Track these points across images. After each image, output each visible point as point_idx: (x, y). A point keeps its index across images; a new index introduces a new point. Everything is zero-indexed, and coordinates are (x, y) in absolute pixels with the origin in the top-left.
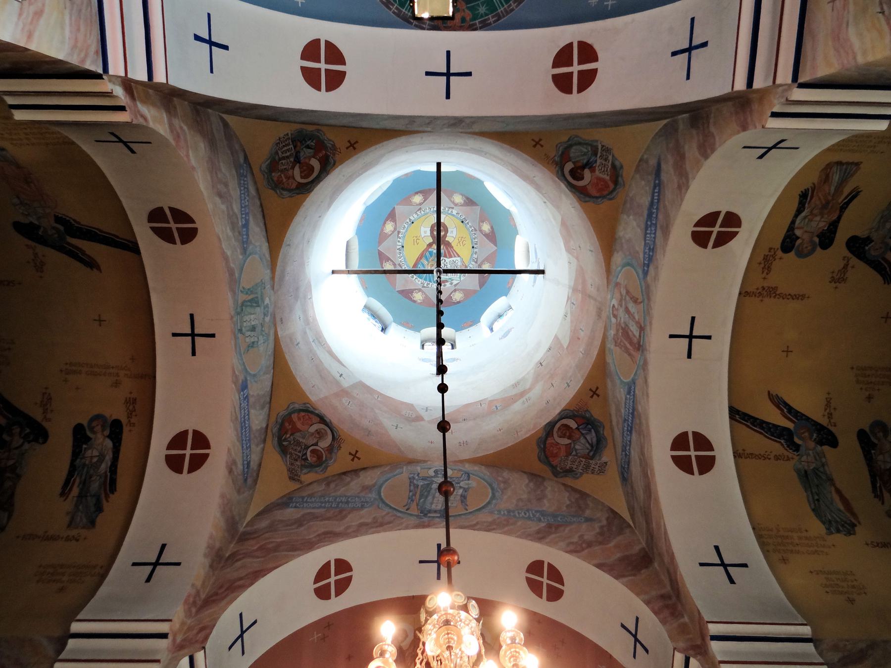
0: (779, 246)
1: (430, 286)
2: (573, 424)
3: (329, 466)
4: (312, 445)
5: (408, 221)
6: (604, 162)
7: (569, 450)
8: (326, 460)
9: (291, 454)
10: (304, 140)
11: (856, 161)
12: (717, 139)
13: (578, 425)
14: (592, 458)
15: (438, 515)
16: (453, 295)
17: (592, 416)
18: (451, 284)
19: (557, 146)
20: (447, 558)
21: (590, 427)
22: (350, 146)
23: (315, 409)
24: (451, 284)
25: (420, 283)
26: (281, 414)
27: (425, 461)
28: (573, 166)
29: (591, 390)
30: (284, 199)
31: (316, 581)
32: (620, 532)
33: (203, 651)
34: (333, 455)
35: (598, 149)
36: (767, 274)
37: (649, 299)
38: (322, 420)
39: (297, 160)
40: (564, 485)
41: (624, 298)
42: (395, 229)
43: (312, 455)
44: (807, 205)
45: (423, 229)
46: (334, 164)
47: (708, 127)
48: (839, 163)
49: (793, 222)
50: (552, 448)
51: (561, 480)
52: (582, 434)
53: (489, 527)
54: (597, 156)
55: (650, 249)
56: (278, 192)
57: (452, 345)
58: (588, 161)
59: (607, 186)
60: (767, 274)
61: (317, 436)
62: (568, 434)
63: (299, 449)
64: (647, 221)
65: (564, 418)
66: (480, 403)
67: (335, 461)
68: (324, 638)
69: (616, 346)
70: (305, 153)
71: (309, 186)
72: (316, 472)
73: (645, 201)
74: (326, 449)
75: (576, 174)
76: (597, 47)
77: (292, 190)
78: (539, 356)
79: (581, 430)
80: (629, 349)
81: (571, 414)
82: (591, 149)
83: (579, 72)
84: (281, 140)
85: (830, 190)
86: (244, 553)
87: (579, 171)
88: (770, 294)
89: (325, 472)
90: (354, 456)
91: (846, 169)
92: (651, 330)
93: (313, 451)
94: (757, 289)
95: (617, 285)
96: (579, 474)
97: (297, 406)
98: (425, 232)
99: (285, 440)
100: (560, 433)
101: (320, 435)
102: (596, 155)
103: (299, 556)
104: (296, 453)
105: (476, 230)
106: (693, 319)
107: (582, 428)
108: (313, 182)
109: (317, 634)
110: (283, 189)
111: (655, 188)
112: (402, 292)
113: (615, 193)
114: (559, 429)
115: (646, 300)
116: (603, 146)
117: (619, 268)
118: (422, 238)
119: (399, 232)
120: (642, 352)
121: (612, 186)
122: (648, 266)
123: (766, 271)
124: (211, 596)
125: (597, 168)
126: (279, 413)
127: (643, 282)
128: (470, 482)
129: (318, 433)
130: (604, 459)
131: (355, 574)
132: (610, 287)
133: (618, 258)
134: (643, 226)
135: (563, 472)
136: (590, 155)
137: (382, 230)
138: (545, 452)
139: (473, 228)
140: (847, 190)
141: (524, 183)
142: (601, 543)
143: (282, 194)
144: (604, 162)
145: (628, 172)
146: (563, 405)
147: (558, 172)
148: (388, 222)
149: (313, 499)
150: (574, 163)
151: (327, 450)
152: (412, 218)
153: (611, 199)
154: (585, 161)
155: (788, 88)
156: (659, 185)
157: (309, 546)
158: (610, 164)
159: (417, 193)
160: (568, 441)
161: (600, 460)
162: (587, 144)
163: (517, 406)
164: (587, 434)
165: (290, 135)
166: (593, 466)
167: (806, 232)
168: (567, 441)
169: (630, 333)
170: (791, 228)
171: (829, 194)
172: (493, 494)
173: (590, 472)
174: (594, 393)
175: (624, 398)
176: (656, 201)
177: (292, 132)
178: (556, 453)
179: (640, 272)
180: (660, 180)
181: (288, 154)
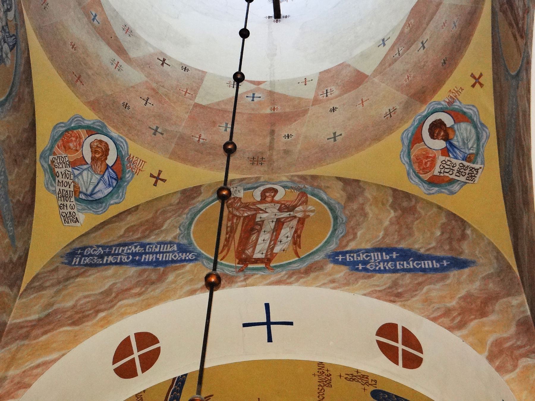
0: (379, 388)
2: (111, 160)
6: (456, 169)
13: (112, 166)
14: (78, 200)
19: (473, 106)
20: (5, 211)
21: (114, 184)
28: (448, 126)
29: (160, 172)
32: (11, 286)
35: (474, 163)
36: (346, 378)
37: (308, 271)
47: (526, 355)
50: (74, 139)
54: (463, 160)
55: (365, 263)
58: (456, 147)
59: (426, 170)
60: (346, 378)
62: (97, 156)
65: (115, 144)
79: (107, 173)
80: (234, 237)
82: (472, 154)
87: (442, 134)
88: (323, 381)
94: (328, 371)
96: (54, 189)
100: (96, 144)
102: (465, 159)
106: (291, 324)
111: (439, 259)
113: (417, 180)
114: (101, 141)
117: (325, 197)
120: (241, 270)
121: (427, 177)
122: (344, 263)
123: (349, 378)
135: (49, 165)
144: (456, 169)
153: (408, 174)
154: (455, 143)
156: (443, 269)
158: (453, 177)
160: (88, 159)
161: (79, 210)
162: (478, 149)
164: (105, 183)
166: (68, 203)
168: (88, 157)
169: (254, 237)
173: (60, 203)
174: (158, 178)
175: (169, 238)
178: (70, 148)
179: (332, 247)
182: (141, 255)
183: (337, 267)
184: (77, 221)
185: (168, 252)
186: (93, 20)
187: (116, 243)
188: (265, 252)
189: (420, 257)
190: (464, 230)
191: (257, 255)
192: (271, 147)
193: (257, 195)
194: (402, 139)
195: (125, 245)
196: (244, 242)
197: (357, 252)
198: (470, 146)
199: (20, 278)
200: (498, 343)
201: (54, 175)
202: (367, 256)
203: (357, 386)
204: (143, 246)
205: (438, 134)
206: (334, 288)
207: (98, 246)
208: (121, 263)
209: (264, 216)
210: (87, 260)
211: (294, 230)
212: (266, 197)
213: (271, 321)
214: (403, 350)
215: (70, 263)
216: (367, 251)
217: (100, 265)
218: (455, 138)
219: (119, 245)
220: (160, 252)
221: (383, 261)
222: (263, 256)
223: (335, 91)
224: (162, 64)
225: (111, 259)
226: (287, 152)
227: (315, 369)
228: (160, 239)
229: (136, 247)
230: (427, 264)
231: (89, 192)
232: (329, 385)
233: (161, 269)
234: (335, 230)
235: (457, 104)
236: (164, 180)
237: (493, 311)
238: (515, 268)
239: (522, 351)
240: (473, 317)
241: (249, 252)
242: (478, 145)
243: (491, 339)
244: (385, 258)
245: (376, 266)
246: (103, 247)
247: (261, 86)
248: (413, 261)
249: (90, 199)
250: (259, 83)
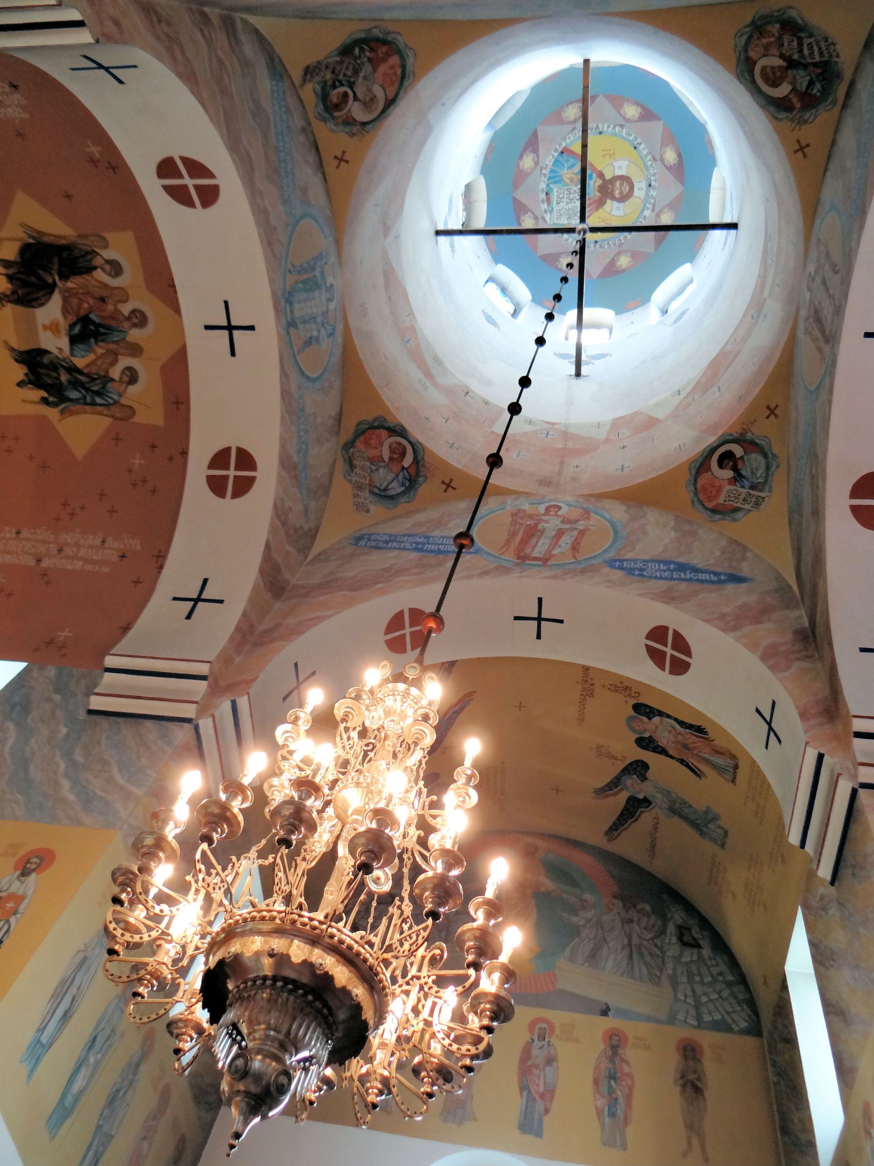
1: (543, 178)
2: (408, 461)
3: (326, 125)
4: (355, 94)
5: (639, 140)
7: (376, 461)
8: (333, 118)
9: (342, 62)
10: (824, 79)
11: (736, 780)
12: (785, 674)
14: (372, 493)
15: (289, 319)
16: (530, 216)
17: (420, 485)
18: (546, 211)
22: (804, 147)
23: (406, 91)
24: (546, 211)
25: (547, 162)
26: (399, 37)
27: (340, 263)
29: (451, 480)
30: (733, 37)
31: (185, 160)
32: (299, 551)
33: (92, 41)
34: (341, 127)
36: (609, 689)
37: (583, 571)
38: (390, 103)
39: (792, 64)
40: (335, 461)
41: (574, 526)
42: (628, 120)
43: (341, 95)
44: (688, 731)
45: (624, 164)
46: (776, 118)
47: (798, 659)
48: (736, 767)
49: (669, 716)
51: (339, 456)
52: (397, 475)
53: (286, 394)
55: (641, 570)
56: (748, 29)
57: (515, 311)
60: (609, 689)
61: (368, 99)
63: (349, 73)
64: (674, 563)
66: (411, 313)
67: (333, 131)
68: (93, 161)
69: (513, 515)
70: (802, 79)
71: (748, 77)
72: (317, 106)
73: (697, 559)
74: (349, 114)
75: (727, 459)
77: (746, 51)
78: (477, 388)
79: (401, 473)
80: (514, 539)
81: (419, 458)
84: (832, 46)
85: (705, 753)
86: (211, 38)
87: (731, 464)
89: (318, 119)
90: (341, 159)
91: (729, 771)
92: (546, 578)
93: (346, 95)
94: (592, 679)
95: (586, 514)
97: (410, 61)
98: (620, 167)
99: (362, 50)
100: (394, 445)
101: (368, 104)
102: (753, 487)
103: (222, 136)
104: (344, 69)
105: (621, 245)
106: (561, 621)
107: (404, 473)
108: (754, 82)
109: (89, 146)
110: (750, 37)
111: (716, 574)
112: (535, 136)
113: (700, 508)
114: (400, 444)
115: (580, 567)
116: (763, 498)
117: (608, 517)
118: (612, 164)
119: (622, 126)
120: (518, 564)
121: (710, 505)
122: (621, 568)
124: (156, 13)
125: (735, 488)
126: (401, 35)
127: (599, 560)
128: (326, 340)
129: (372, 100)
130: (372, 508)
131: (199, 211)
132: (581, 500)
133: (618, 512)
134: (667, 556)
136: (751, 480)
137: (628, 100)
138: (370, 428)
139: (623, 241)
140: (702, 767)
141: (706, 361)
142: (287, 534)
143: (742, 35)
144: (742, 497)
145: (729, 527)
146: (429, 444)
147: (731, 435)
148: (639, 110)
149: (284, 116)
150: (742, 458)
151: (348, 117)
152: (643, 146)
153: (693, 502)
154: (743, 472)
155: (855, 777)
156: (720, 582)
157: (234, 145)
158: (738, 505)
159: (679, 155)
160: (386, 458)
161: (371, 502)
163: (415, 373)
164: (398, 481)
165: (837, 60)
167: (657, 727)
169: (534, 540)
170: (661, 714)
171: (700, 752)
172: (316, 379)
173: (355, 492)
174: (448, 486)
176: (700, 578)
177: (840, 64)
179: (611, 555)
180: (725, 581)
181: (806, 52)
182: (424, 544)
183: (614, 571)
184: (368, 511)
185: (448, 545)
186: (408, 342)
187: (401, 533)
188: (543, 553)
189: (697, 570)
191: (535, 554)
192: (560, 473)
193: (542, 509)
194: (690, 470)
195: (409, 536)
196: (524, 542)
197: (635, 561)
198: (758, 475)
199: (309, 548)
201: (352, 466)
202: (644, 565)
203: (619, 698)
204: (428, 538)
205: (728, 464)
206: (608, 587)
207: (385, 534)
208: (404, 549)
209: (546, 525)
210: (373, 544)
211: (574, 538)
212: (550, 511)
214: (671, 655)
215: (356, 544)
216: (645, 561)
217: (384, 548)
218: (744, 468)
219: (404, 535)
220: (442, 544)
221: (661, 570)
222: (542, 556)
223: (627, 433)
224: (465, 395)
225: (395, 544)
226: (573, 479)
228: (444, 534)
229: (420, 538)
230: (704, 577)
231: (382, 488)
232: (592, 695)
233: (442, 556)
234: (614, 542)
235: (749, 436)
236: (454, 488)
240: (747, 623)
241: (528, 551)
242: (767, 475)
243: (765, 643)
244: (662, 568)
245: (652, 573)
246: (390, 535)
247: (556, 427)
248: (691, 573)
249: (383, 494)
250: (553, 424)
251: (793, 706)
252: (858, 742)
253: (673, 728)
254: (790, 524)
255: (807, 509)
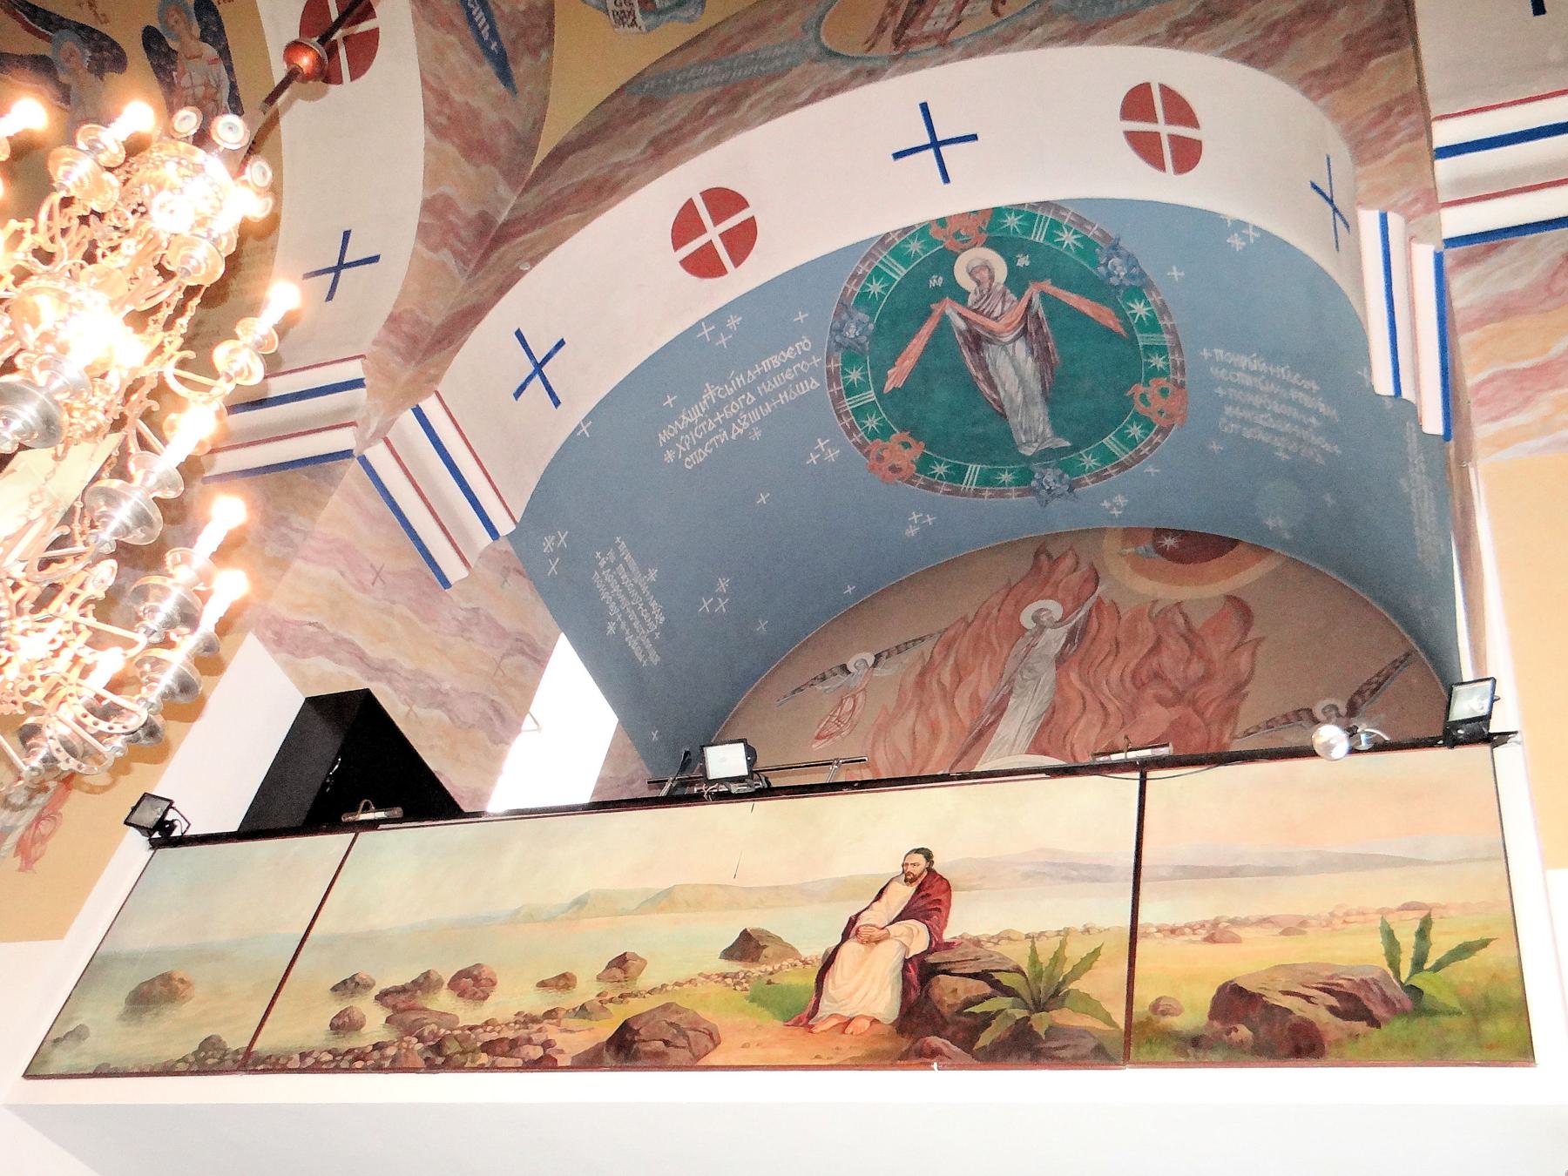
12: (427, 254)
47: (455, 253)
49: (230, 70)
76: (694, 279)
83: (722, 236)
111: (494, 33)
116: (634, 23)
156: (485, 46)
170: (225, 54)
190: (542, 46)
200: (448, 203)
213: (939, 140)
227: (312, 714)
237: (477, 166)
238: (537, 160)
239: (459, 245)
243: (446, 189)
251: (394, 296)
252: (408, 417)
253: (218, 86)
254: (619, 91)
255: (657, 124)
